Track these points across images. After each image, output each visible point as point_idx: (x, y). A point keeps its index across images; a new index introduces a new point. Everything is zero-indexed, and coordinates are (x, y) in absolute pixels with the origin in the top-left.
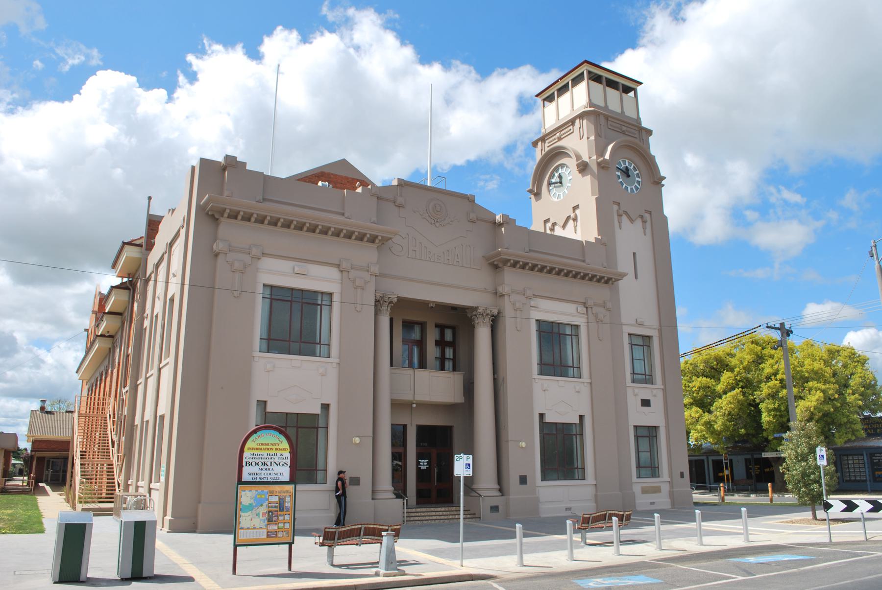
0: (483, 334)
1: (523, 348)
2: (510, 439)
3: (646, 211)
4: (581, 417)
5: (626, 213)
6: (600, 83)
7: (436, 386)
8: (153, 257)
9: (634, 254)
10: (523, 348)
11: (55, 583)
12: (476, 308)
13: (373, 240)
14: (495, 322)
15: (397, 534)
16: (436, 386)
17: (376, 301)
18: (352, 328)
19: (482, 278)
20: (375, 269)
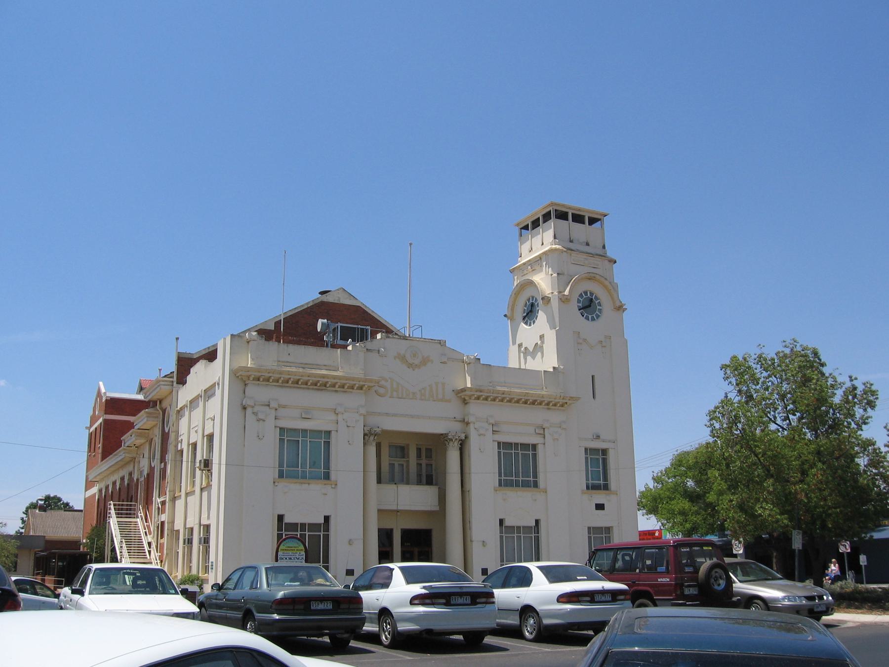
0: (453, 456)
1: (484, 464)
2: (474, 539)
3: (606, 337)
4: (537, 522)
5: (585, 340)
6: (567, 219)
7: (414, 498)
8: (185, 395)
9: (593, 377)
10: (484, 464)
11: (140, 383)
12: (446, 435)
13: (361, 388)
14: (463, 446)
15: (158, 381)
16: (414, 498)
17: (365, 435)
18: (350, 458)
19: (454, 409)
20: (363, 411)
